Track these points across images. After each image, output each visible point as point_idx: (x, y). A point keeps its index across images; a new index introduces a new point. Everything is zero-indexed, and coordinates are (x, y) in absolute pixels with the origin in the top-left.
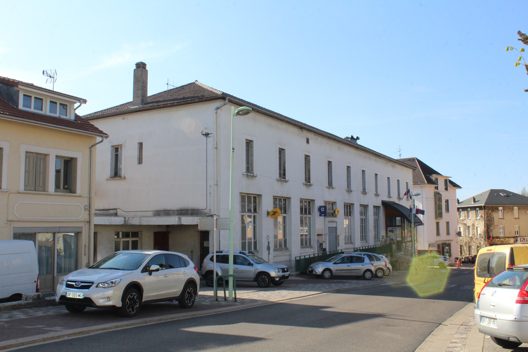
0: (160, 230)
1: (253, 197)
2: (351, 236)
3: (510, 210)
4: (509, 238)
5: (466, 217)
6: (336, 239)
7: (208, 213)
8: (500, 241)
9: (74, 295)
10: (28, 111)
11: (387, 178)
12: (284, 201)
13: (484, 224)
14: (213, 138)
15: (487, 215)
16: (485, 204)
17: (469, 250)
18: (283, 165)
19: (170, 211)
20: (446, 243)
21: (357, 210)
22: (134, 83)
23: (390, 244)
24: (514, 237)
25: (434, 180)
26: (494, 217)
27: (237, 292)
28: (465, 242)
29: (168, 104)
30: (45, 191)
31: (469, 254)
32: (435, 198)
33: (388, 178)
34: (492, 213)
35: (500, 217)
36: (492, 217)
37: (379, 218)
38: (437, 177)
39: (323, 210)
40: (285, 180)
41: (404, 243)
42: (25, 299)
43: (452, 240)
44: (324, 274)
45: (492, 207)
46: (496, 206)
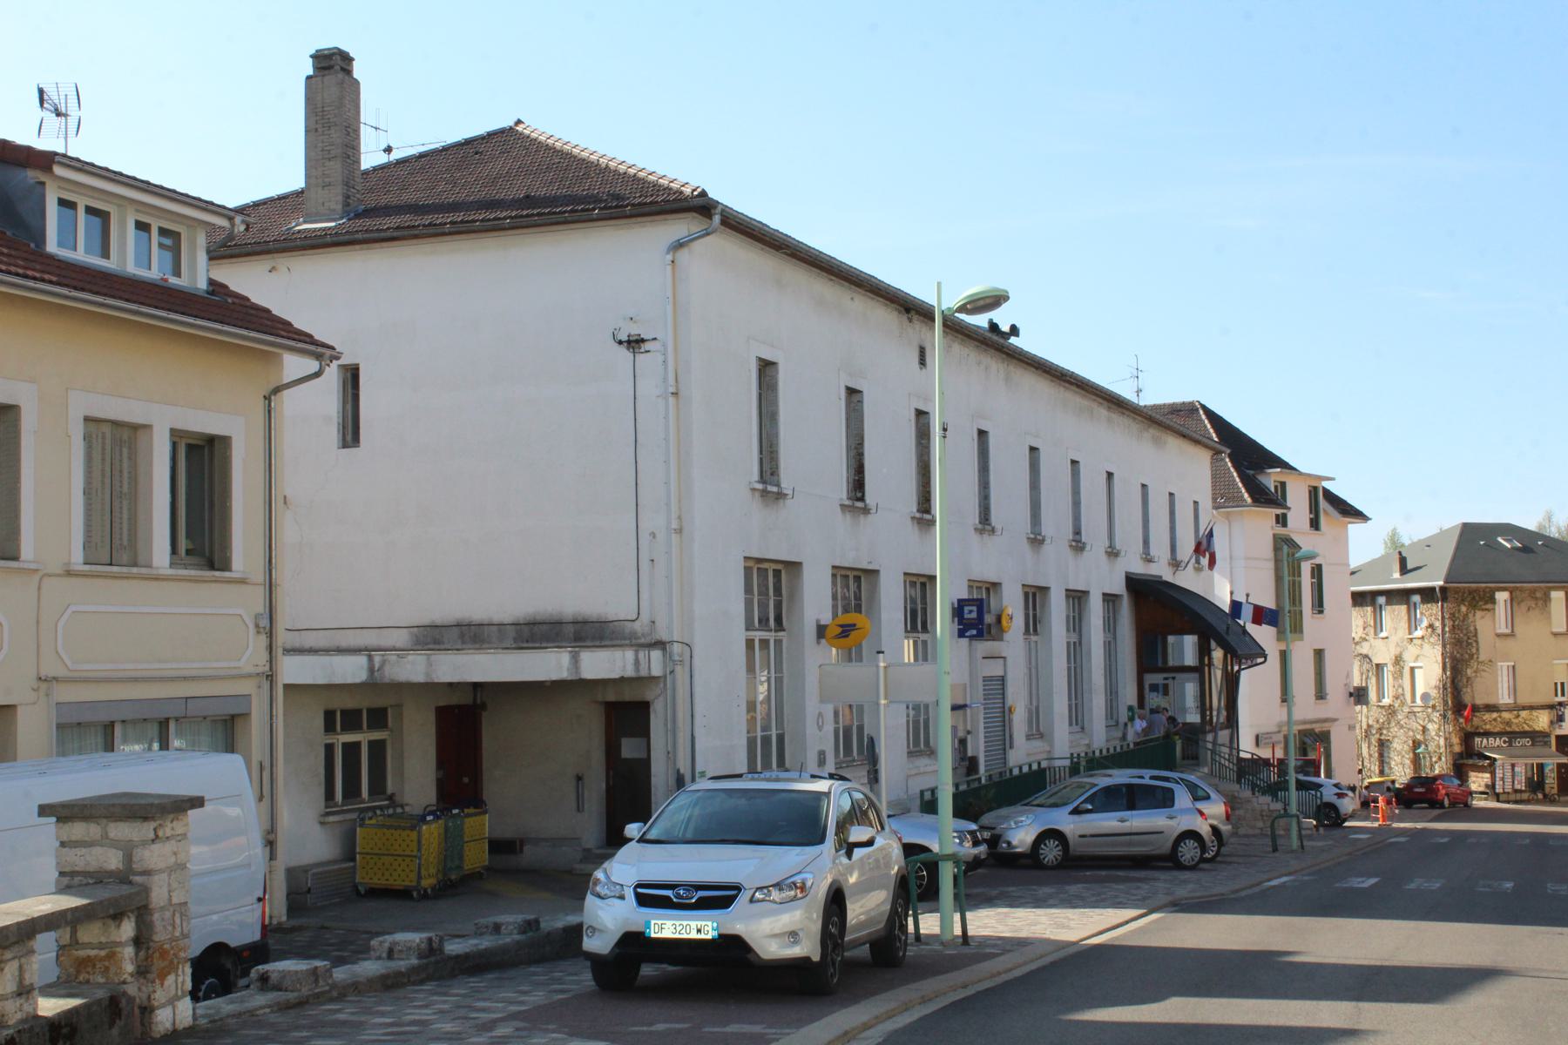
0: (455, 699)
1: (774, 570)
2: (1037, 708)
3: (1536, 604)
4: (1531, 708)
5: (1372, 631)
6: (1004, 721)
7: (643, 635)
8: (1501, 723)
9: (679, 929)
10: (70, 261)
11: (1140, 487)
12: (856, 584)
13: (1439, 658)
14: (660, 358)
15: (1454, 622)
16: (1445, 582)
17: (1381, 755)
18: (856, 448)
19: (486, 627)
20: (1313, 730)
21: (1057, 608)
22: (308, 131)
23: (1167, 736)
24: (1551, 707)
25: (1273, 490)
26: (1479, 631)
27: (969, 915)
28: (1364, 726)
29: (474, 221)
30: (135, 565)
31: (1382, 773)
32: (1277, 561)
33: (1144, 486)
34: (1470, 615)
35: (1499, 631)
36: (1472, 628)
37: (1115, 638)
38: (1283, 480)
39: (971, 613)
40: (859, 504)
41: (1210, 731)
42: (384, 955)
43: (1335, 720)
44: (1041, 852)
45: (1470, 593)
46: (1487, 587)
